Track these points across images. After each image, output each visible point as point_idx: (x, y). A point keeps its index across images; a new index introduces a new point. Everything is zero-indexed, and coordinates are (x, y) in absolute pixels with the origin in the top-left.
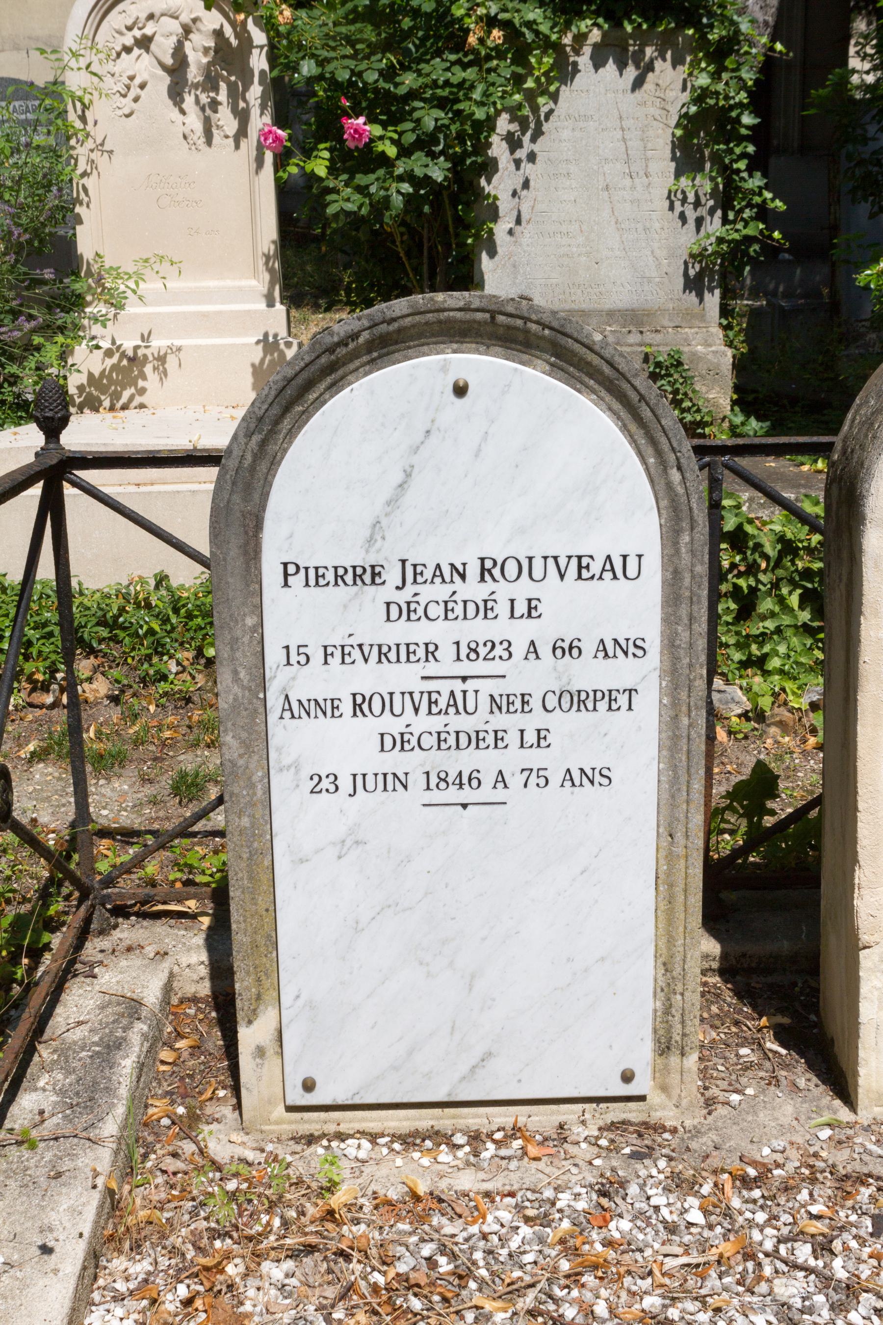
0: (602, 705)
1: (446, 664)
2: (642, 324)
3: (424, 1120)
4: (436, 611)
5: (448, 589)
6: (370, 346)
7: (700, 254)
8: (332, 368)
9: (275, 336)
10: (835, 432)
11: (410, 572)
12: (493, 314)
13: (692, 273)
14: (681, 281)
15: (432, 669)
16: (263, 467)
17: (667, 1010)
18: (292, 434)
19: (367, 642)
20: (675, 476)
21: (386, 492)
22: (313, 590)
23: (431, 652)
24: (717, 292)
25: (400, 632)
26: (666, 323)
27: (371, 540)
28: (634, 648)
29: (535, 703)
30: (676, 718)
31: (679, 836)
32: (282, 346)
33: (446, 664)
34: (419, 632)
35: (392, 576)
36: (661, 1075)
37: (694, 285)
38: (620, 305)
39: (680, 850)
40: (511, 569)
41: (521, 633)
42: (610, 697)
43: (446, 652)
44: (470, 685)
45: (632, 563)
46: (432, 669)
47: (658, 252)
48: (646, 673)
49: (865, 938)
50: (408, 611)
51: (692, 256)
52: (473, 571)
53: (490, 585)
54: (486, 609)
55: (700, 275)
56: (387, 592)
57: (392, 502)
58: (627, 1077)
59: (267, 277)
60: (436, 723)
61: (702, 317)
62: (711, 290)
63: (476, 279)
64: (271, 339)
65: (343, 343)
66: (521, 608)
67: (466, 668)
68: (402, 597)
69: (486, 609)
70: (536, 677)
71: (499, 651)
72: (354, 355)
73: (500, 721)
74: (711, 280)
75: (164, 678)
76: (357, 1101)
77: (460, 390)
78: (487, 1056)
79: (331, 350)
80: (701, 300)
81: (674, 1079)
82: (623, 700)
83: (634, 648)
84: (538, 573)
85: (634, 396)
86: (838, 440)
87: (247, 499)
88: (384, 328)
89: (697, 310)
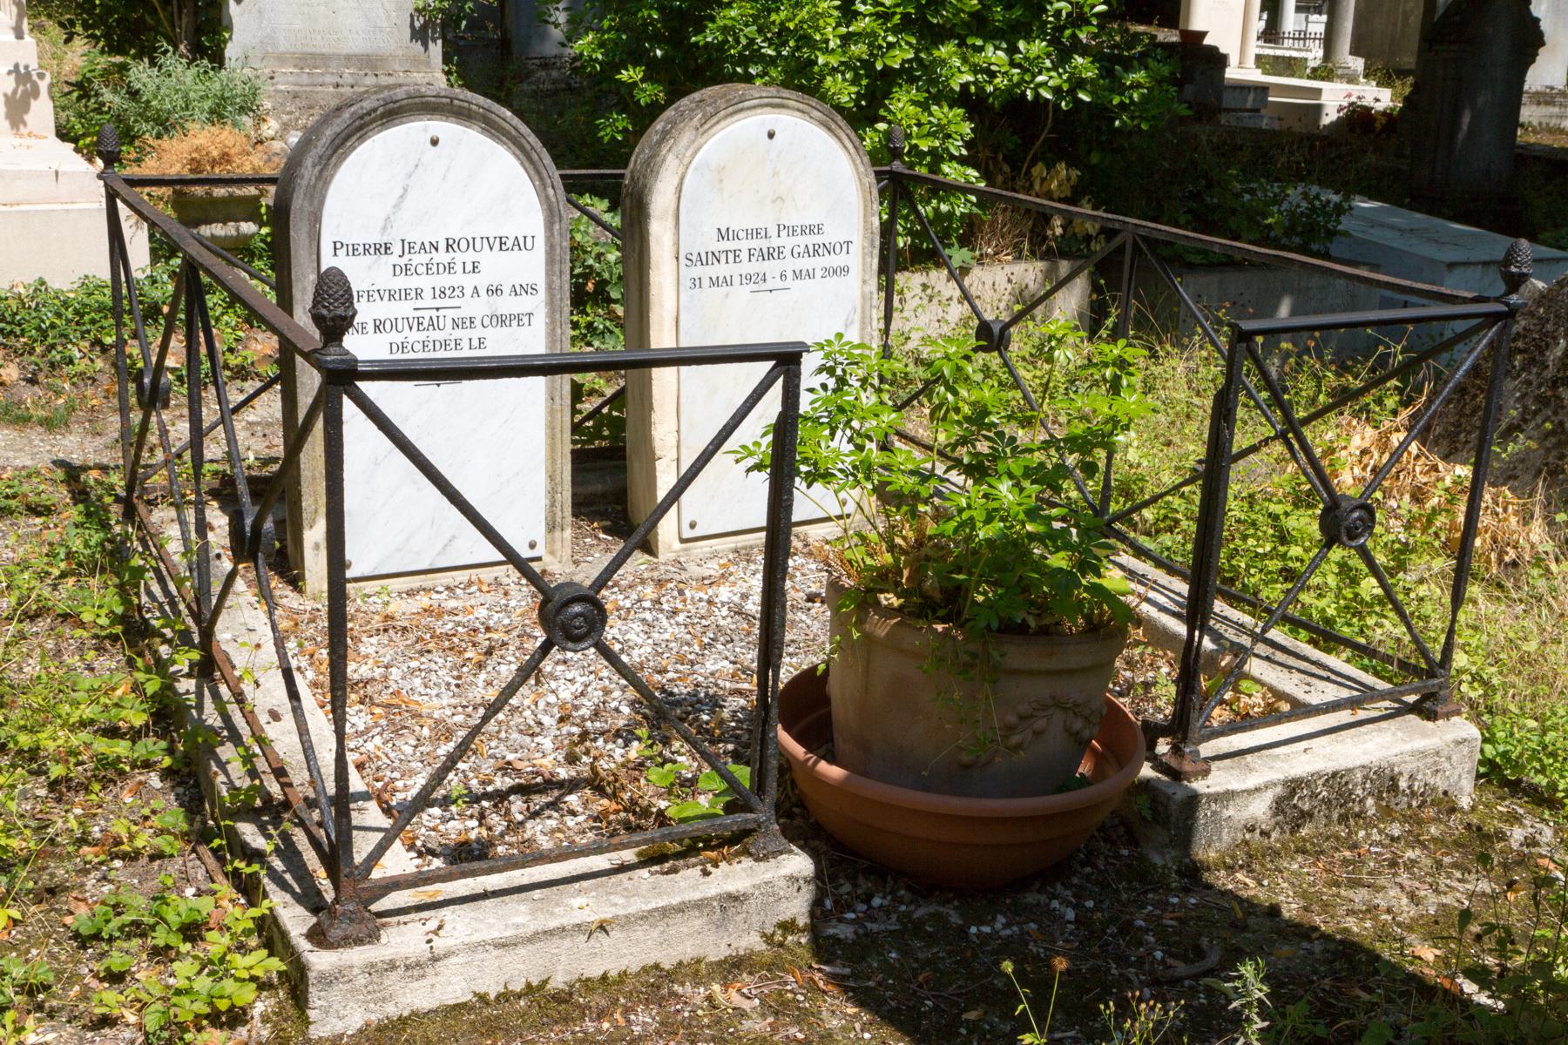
0: (515, 323)
1: (427, 301)
2: (376, 68)
3: (415, 582)
4: (422, 269)
5: (428, 256)
6: (382, 116)
7: (424, 9)
8: (361, 128)
9: (26, 67)
10: (626, 167)
11: (408, 247)
12: (452, 99)
13: (417, 25)
14: (408, 31)
15: (419, 304)
16: (320, 185)
17: (553, 505)
18: (337, 166)
19: (382, 288)
20: (551, 191)
21: (393, 201)
22: (351, 258)
23: (419, 294)
24: (439, 42)
25: (402, 282)
26: (396, 67)
27: (384, 228)
28: (529, 289)
29: (478, 323)
30: (553, 330)
31: (557, 399)
32: (35, 77)
33: (427, 301)
34: (412, 282)
35: (397, 249)
36: (550, 543)
37: (420, 35)
38: (356, 51)
39: (558, 407)
40: (463, 245)
41: (469, 281)
42: (519, 318)
43: (428, 294)
44: (441, 313)
45: (529, 241)
46: (419, 304)
47: (387, 6)
48: (537, 304)
49: (658, 453)
50: (406, 269)
51: (417, 10)
52: (442, 246)
53: (452, 254)
54: (449, 268)
55: (424, 27)
56: (394, 259)
57: (397, 206)
58: (532, 546)
59: (15, 10)
60: (422, 336)
61: (428, 64)
62: (434, 40)
63: (225, 23)
64: (22, 70)
65: (369, 114)
66: (469, 267)
67: (439, 303)
68: (402, 262)
69: (449, 268)
70: (477, 307)
71: (457, 292)
72: (373, 121)
73: (458, 333)
74: (434, 32)
75: (71, 362)
76: (376, 573)
77: (435, 142)
78: (454, 537)
79: (361, 118)
80: (426, 49)
81: (558, 545)
82: (525, 320)
83: (529, 289)
84: (478, 247)
85: (528, 147)
86: (627, 172)
87: (311, 204)
88: (391, 106)
89: (423, 57)
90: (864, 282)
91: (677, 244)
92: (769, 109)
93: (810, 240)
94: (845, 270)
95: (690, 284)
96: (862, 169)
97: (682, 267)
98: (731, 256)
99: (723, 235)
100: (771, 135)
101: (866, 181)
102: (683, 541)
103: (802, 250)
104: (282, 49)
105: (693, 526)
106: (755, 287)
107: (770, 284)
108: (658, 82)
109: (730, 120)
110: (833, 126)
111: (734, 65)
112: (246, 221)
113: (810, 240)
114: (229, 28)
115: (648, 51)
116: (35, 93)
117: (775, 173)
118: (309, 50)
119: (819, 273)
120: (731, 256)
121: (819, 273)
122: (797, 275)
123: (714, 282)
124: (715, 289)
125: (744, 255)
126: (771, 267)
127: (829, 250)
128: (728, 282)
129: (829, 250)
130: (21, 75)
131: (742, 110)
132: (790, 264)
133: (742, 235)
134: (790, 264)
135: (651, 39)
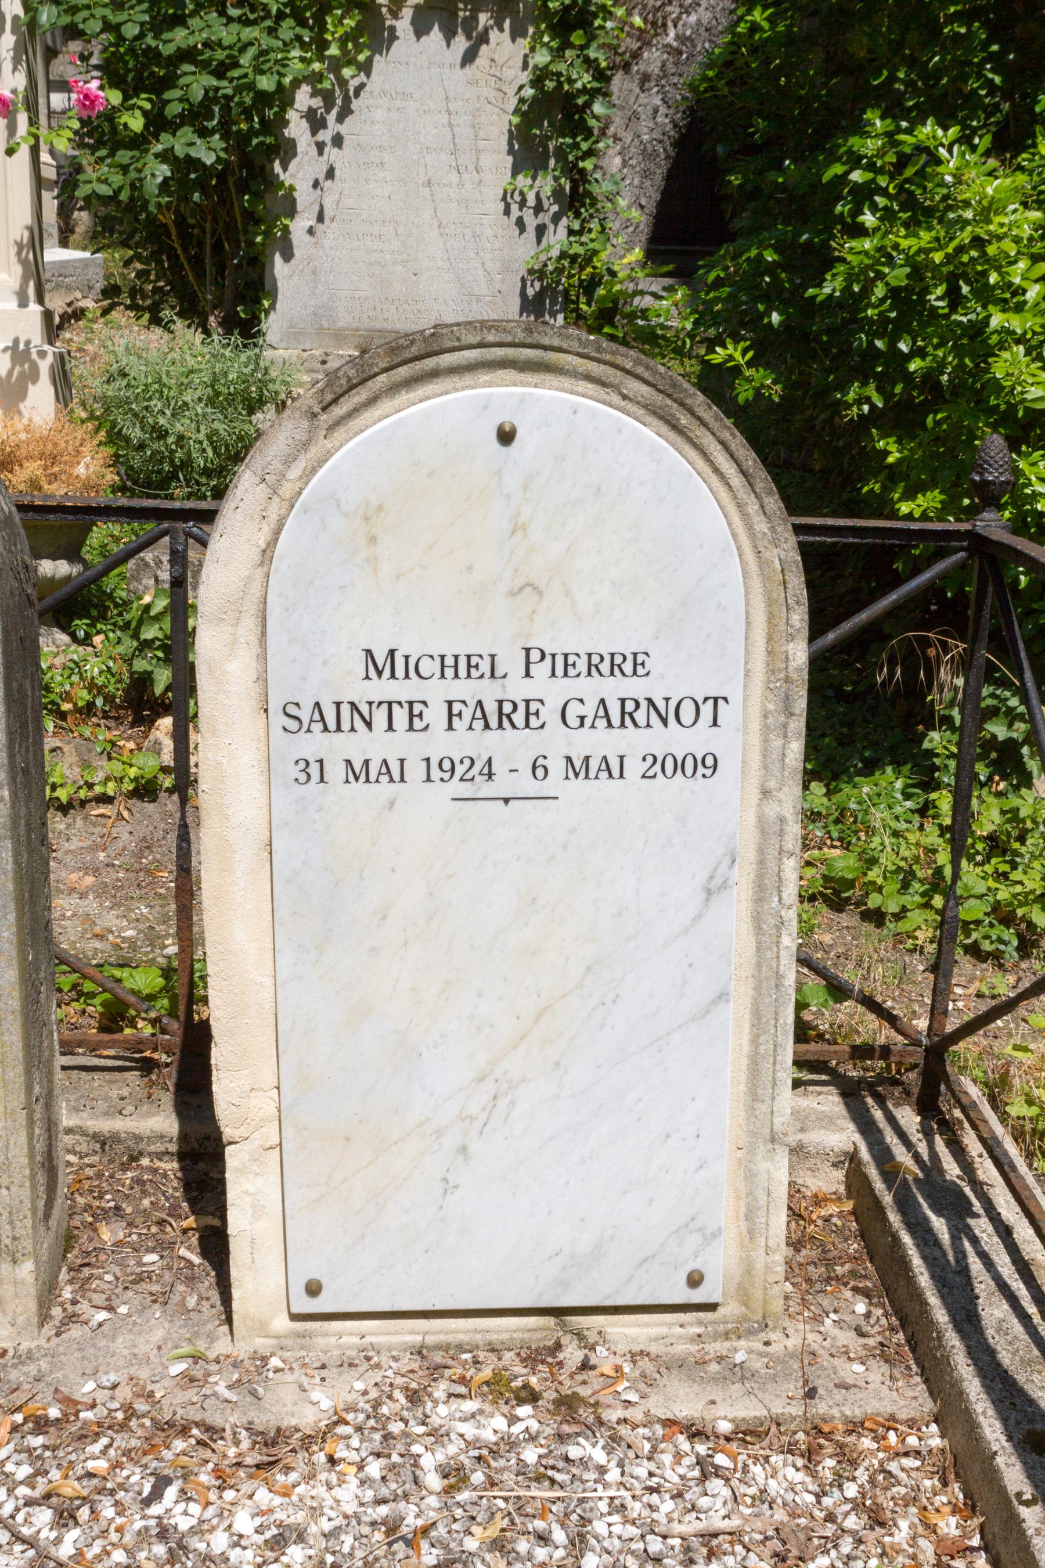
9: (28, 343)
13: (530, 292)
14: (517, 302)
32: (34, 356)
47: (489, 265)
49: (228, 1132)
51: (531, 271)
55: (540, 296)
59: (18, 270)
74: (553, 303)
90: (765, 793)
91: (262, 678)
92: (511, 374)
93: (614, 689)
94: (707, 765)
95: (295, 772)
96: (762, 526)
97: (277, 732)
98: (400, 716)
99: (379, 664)
100: (506, 436)
101: (773, 555)
102: (295, 1317)
103: (589, 709)
104: (341, 324)
105: (313, 1289)
106: (465, 790)
107: (500, 786)
108: (767, 366)
109: (404, 397)
110: (684, 420)
111: (873, 335)
112: (54, 558)
113: (614, 689)
114: (273, 295)
115: (762, 316)
116: (34, 376)
117: (518, 528)
118: (379, 325)
119: (635, 768)
120: (400, 716)
121: (635, 768)
122: (577, 768)
123: (358, 772)
124: (361, 786)
125: (435, 715)
126: (509, 747)
127: (665, 714)
128: (393, 772)
129: (665, 714)
130: (19, 353)
131: (434, 374)
132: (557, 743)
133: (428, 667)
134: (557, 743)
135: (766, 298)
